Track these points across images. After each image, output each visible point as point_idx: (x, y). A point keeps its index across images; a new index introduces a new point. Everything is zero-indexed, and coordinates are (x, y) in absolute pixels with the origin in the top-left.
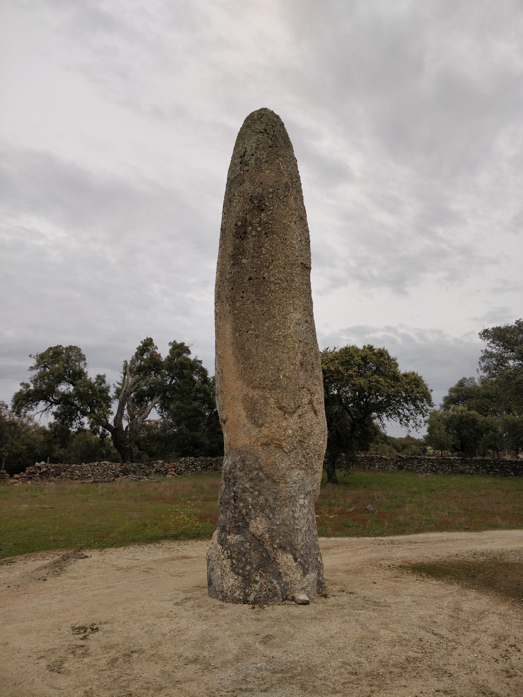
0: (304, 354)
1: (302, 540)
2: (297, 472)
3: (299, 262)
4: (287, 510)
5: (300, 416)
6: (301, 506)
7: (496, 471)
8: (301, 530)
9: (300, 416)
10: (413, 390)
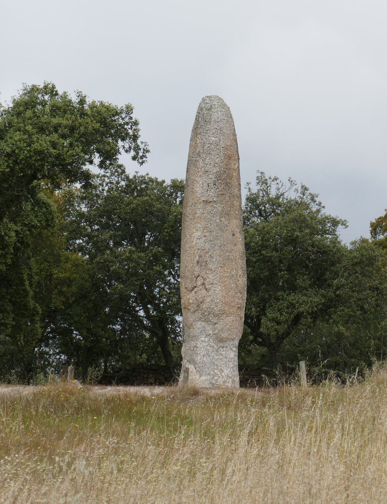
0: (200, 256)
1: (200, 359)
2: (200, 323)
3: (201, 200)
4: (193, 342)
5: (196, 292)
6: (202, 341)
7: (102, 247)
8: (200, 354)
9: (196, 292)
10: (139, 156)
